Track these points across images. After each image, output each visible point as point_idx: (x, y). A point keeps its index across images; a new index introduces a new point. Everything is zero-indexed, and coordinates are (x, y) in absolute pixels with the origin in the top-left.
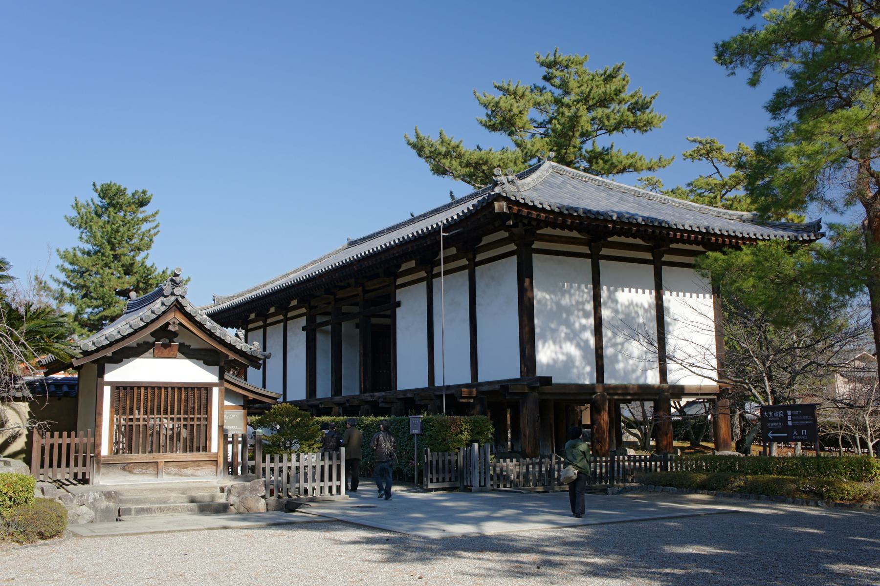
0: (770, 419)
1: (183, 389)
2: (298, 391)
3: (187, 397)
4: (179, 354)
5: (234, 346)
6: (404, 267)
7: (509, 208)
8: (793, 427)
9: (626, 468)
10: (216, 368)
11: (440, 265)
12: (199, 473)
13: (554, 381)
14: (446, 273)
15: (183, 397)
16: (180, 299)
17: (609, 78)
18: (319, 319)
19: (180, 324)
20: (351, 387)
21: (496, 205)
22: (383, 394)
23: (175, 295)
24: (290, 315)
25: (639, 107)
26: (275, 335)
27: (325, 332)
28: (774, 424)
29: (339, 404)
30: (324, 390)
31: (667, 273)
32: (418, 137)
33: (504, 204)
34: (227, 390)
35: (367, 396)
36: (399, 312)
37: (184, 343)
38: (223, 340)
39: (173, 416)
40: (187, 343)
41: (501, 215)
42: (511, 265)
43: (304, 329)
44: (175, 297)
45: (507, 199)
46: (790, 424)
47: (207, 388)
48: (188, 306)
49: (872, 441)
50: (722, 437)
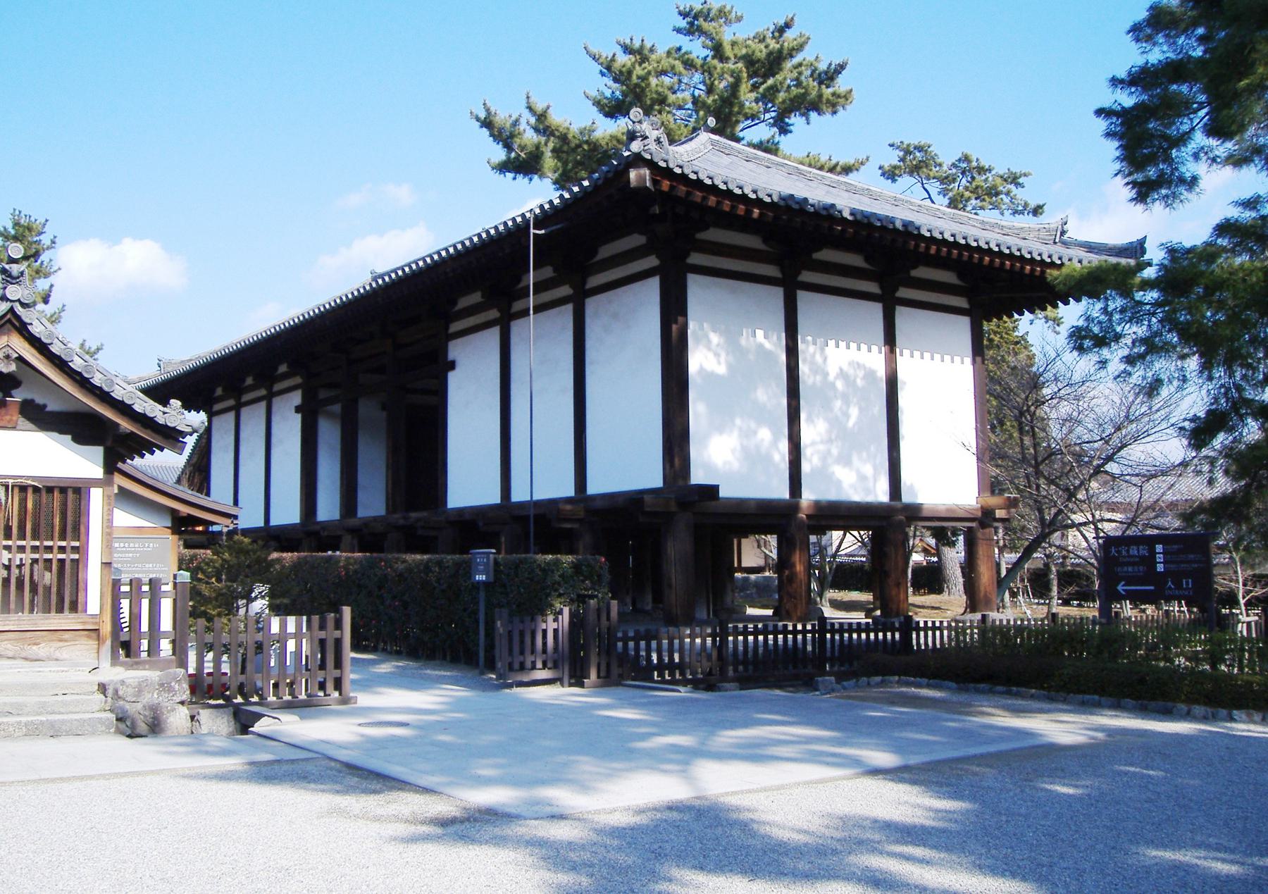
0: (1121, 559)
1: (30, 491)
2: (287, 512)
3: (37, 505)
4: (22, 422)
5: (129, 407)
6: (464, 302)
7: (654, 182)
8: (1166, 573)
9: (855, 642)
10: (98, 451)
11: (529, 296)
12: (64, 654)
13: (723, 493)
14: (539, 309)
15: (30, 505)
16: (19, 309)
17: (781, 30)
18: (323, 394)
19: (21, 359)
20: (372, 504)
21: (633, 174)
22: (424, 514)
23: (8, 300)
24: (277, 387)
25: (828, 77)
26: (253, 419)
27: (331, 415)
28: (1130, 569)
29: (353, 531)
30: (328, 509)
31: (903, 316)
32: (488, 110)
33: (646, 172)
34: (123, 493)
35: (397, 518)
36: (453, 377)
37: (32, 401)
38: (108, 394)
39: (10, 543)
40: (40, 400)
41: (642, 190)
42: (647, 297)
43: (298, 409)
44: (8, 305)
45: (651, 164)
46: (1160, 568)
47: (74, 492)
48: (35, 323)
49: (1244, 598)
50: (982, 589)
